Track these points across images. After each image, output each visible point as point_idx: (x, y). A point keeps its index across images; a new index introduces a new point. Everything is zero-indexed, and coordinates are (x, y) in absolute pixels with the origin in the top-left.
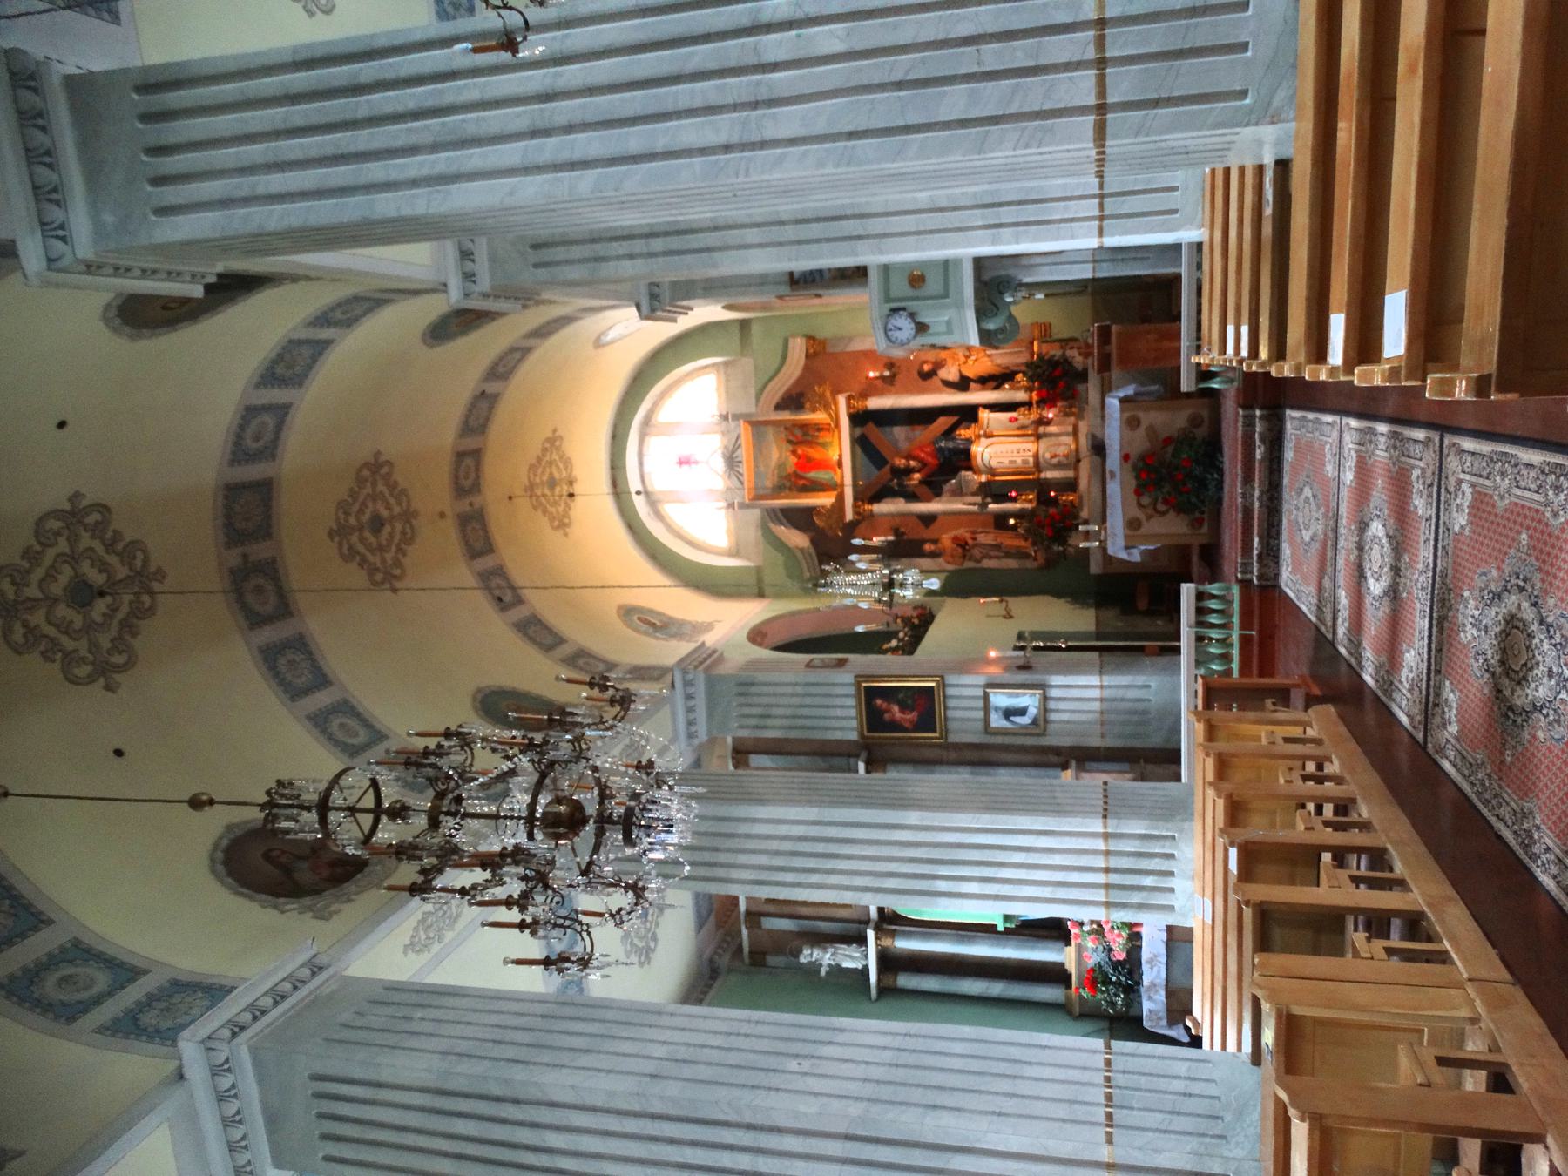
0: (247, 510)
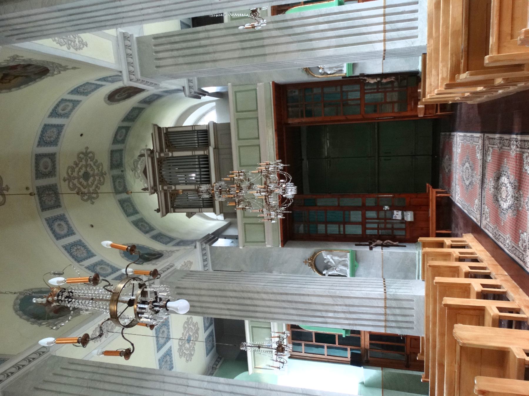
0: (44, 165)
